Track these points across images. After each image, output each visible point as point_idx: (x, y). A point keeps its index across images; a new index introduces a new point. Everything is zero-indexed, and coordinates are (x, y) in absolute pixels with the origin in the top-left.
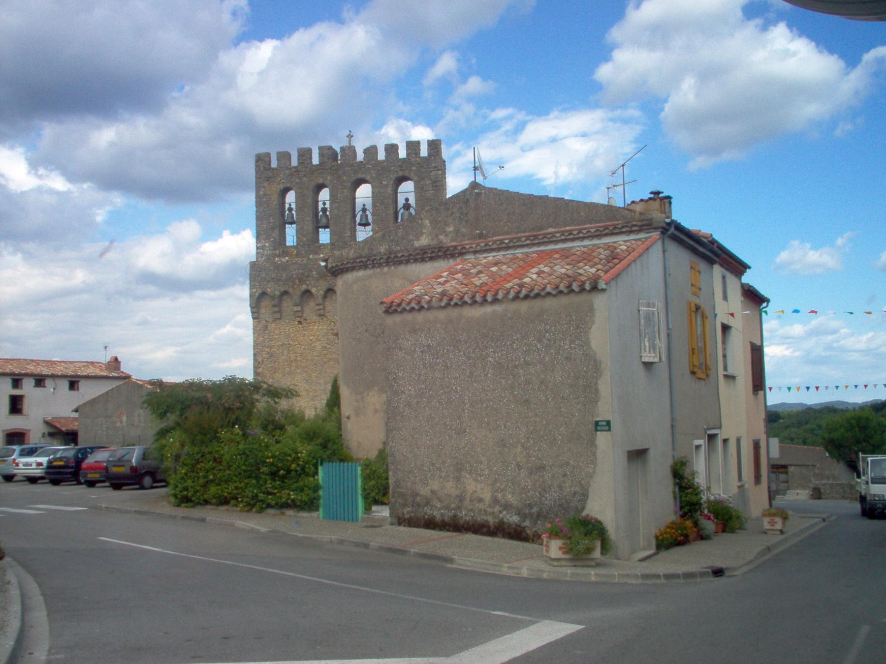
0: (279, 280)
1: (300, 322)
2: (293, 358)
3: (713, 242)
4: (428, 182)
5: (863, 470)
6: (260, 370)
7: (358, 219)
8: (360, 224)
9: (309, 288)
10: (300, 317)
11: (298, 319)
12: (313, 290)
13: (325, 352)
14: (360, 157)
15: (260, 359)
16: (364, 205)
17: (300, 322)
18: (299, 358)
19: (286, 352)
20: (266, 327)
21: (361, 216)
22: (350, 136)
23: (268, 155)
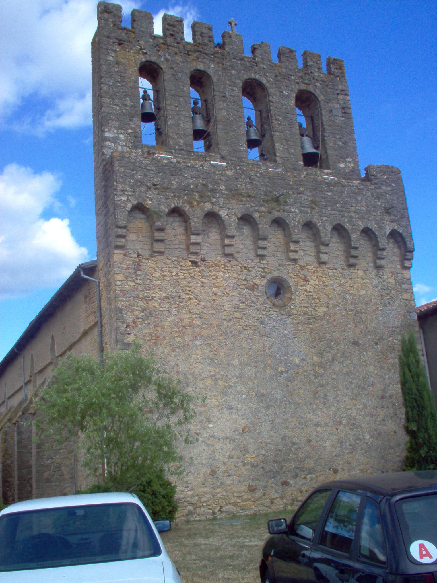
0: (166, 189)
2: (186, 322)
3: (285, 561)
4: (337, 106)
9: (216, 209)
10: (196, 254)
11: (193, 258)
12: (223, 213)
13: (237, 315)
17: (194, 263)
18: (197, 322)
19: (174, 311)
20: (138, 266)
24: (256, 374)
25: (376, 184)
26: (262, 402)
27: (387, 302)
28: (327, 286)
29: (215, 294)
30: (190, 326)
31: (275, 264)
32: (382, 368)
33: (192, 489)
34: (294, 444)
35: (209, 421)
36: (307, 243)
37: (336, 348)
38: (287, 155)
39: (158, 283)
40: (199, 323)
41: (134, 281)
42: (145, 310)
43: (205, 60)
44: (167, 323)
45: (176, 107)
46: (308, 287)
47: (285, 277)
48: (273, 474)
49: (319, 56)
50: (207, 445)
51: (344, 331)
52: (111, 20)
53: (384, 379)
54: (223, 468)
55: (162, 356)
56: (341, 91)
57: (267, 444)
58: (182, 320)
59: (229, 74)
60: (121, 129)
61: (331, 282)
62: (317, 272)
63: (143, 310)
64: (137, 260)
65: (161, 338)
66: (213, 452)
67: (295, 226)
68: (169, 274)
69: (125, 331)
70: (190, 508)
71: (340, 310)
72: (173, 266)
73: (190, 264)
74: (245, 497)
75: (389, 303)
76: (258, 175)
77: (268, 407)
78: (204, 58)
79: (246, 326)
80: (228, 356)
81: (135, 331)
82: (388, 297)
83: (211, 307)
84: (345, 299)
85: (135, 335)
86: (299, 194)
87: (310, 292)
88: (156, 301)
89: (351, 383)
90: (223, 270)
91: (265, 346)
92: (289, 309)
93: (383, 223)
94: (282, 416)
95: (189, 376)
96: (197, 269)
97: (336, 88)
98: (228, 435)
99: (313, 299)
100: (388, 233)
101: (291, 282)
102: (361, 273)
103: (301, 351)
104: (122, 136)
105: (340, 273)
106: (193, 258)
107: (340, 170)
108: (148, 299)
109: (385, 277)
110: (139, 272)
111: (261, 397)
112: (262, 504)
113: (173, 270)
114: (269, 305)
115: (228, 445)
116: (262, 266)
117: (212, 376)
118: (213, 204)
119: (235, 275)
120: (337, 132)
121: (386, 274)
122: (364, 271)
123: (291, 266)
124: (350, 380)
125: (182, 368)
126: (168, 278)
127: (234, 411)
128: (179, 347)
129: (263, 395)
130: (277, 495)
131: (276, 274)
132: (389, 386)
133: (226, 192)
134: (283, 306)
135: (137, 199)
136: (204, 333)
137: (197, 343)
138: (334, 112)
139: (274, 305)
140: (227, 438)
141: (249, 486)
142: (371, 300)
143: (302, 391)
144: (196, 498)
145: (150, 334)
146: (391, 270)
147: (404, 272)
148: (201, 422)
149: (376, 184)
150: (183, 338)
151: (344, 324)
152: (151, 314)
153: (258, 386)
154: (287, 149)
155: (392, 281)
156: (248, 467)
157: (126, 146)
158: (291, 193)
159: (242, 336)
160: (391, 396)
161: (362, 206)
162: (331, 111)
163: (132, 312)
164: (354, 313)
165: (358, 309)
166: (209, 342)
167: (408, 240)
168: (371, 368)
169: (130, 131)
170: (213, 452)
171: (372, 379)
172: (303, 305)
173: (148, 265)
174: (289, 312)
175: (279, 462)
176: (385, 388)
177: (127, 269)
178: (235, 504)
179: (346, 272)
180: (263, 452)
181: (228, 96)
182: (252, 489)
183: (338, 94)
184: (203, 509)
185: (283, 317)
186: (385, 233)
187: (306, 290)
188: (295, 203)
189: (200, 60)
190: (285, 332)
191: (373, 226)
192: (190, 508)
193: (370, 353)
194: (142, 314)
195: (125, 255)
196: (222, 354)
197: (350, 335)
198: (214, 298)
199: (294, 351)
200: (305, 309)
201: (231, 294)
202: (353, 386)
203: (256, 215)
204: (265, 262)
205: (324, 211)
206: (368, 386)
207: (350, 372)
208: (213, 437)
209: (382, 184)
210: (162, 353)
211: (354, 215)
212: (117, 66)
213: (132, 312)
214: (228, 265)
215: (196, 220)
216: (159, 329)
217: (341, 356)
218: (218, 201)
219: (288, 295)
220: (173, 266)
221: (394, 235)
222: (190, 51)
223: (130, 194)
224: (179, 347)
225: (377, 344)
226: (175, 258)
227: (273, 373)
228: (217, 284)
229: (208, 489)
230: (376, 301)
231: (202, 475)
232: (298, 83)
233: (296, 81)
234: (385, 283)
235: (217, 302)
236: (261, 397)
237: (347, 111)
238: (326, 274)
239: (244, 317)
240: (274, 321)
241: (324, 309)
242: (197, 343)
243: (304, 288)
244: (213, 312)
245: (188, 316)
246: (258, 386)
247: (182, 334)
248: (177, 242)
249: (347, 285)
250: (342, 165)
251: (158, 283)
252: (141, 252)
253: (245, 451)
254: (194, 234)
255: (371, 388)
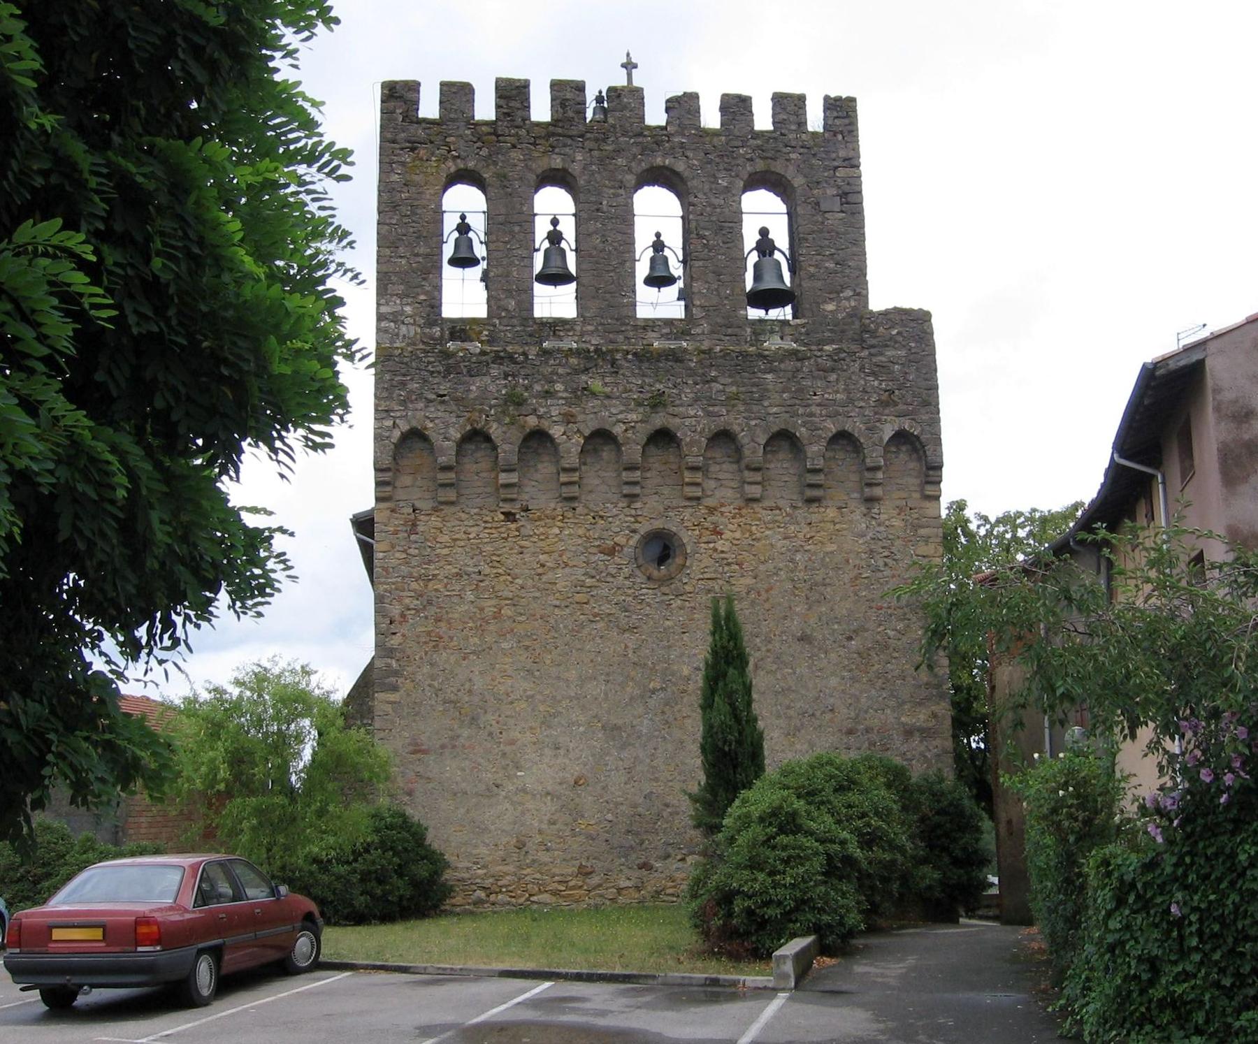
1: (509, 516)
2: (489, 611)
5: (579, 1009)
6: (395, 641)
7: (448, 251)
8: (454, 262)
9: (545, 424)
13: (578, 597)
14: (655, 116)
15: (395, 610)
16: (658, 235)
17: (509, 516)
19: (470, 596)
20: (413, 527)
21: (653, 260)
22: (629, 66)
23: (414, 87)
24: (606, 694)
25: (873, 346)
26: (614, 739)
27: (881, 563)
28: (758, 540)
29: (543, 566)
30: (495, 618)
31: (655, 511)
32: (854, 680)
33: (484, 867)
34: (667, 805)
35: (518, 768)
36: (724, 466)
37: (764, 649)
38: (715, 300)
39: (446, 551)
40: (509, 613)
41: (405, 551)
42: (421, 596)
43: (567, 150)
44: (456, 616)
45: (506, 243)
46: (720, 545)
47: (674, 529)
48: (626, 851)
49: (801, 99)
50: (513, 803)
51: (785, 618)
52: (398, 111)
53: (858, 700)
54: (539, 839)
55: (446, 666)
56: (845, 160)
57: (617, 804)
58: (482, 609)
59: (611, 167)
60: (408, 296)
61: (768, 532)
62: (741, 516)
63: (419, 596)
64: (412, 517)
65: (446, 639)
66: (523, 813)
67: (692, 443)
68: (464, 536)
69: (388, 629)
70: (482, 894)
71: (781, 581)
72: (471, 523)
73: (502, 517)
74: (571, 884)
75: (886, 565)
76: (630, 357)
77: (623, 747)
78: (565, 145)
79: (596, 615)
80: (559, 665)
81: (404, 629)
82: (886, 554)
83: (534, 587)
84: (792, 560)
85: (404, 635)
86: (708, 382)
87: (722, 552)
88: (441, 580)
89: (788, 707)
90: (559, 524)
91: (626, 647)
92: (679, 584)
93: (879, 420)
94: (648, 761)
95: (487, 697)
96: (513, 526)
97: (834, 155)
98: (549, 788)
99: (729, 564)
100: (886, 438)
101: (686, 537)
102: (831, 513)
103: (695, 655)
104: (408, 309)
105: (788, 515)
106: (507, 507)
107: (826, 317)
108: (427, 579)
109: (883, 517)
110: (413, 537)
111: (613, 730)
112: (601, 896)
113: (470, 530)
114: (640, 578)
115: (549, 804)
116: (633, 512)
117: (528, 697)
118: (540, 417)
119: (581, 532)
120: (827, 242)
121: (886, 511)
122: (840, 508)
123: (690, 510)
124: (787, 702)
125: (479, 683)
126: (462, 543)
127: (562, 752)
128: (474, 653)
129: (616, 728)
130: (628, 883)
131: (658, 524)
132: (866, 712)
133: (565, 395)
134: (670, 579)
135: (409, 422)
136: (520, 629)
137: (505, 645)
138: (824, 207)
139: (649, 578)
140: (548, 794)
141: (581, 866)
142: (848, 561)
143: (690, 721)
144: (491, 880)
145: (429, 633)
146: (898, 503)
147: (927, 504)
148: (504, 768)
149: (873, 346)
150: (482, 637)
151: (786, 605)
152: (430, 603)
153: (608, 712)
154: (716, 290)
155: (897, 523)
156: (581, 839)
157: (414, 324)
158: (690, 382)
159: (586, 631)
160: (868, 730)
161: (837, 392)
162: (818, 204)
163: (400, 600)
164: (807, 586)
165: (819, 579)
166: (527, 643)
167: (929, 449)
168: (834, 681)
169: (422, 297)
170: (523, 813)
171: (832, 700)
172: (706, 576)
173: (428, 524)
174: (677, 589)
175: (637, 834)
176: (857, 715)
177: (396, 532)
178: (555, 893)
179: (800, 514)
180: (609, 817)
181: (605, 208)
182: (585, 873)
183: (836, 168)
184: (500, 897)
185: (666, 598)
186: (881, 439)
187: (715, 550)
188: (696, 400)
189: (557, 150)
190: (668, 623)
191: (856, 426)
192: (482, 894)
193: (833, 656)
194: (416, 602)
195: (393, 511)
196: (548, 662)
197: (795, 625)
198: (540, 571)
199: (682, 655)
200: (710, 582)
201: (571, 563)
202: (791, 712)
203: (618, 430)
204: (638, 505)
205: (755, 408)
206: (824, 712)
207: (789, 689)
208: (524, 790)
209: (887, 346)
210: (447, 661)
211: (814, 409)
212: (405, 189)
213: (400, 600)
214: (570, 514)
215: (506, 447)
216: (442, 624)
217: (774, 662)
218: (549, 412)
219: (679, 560)
220: (471, 523)
221: (901, 437)
222: (539, 137)
223: (398, 414)
224: (474, 653)
225: (850, 638)
226: (476, 510)
227: (637, 692)
228: (547, 549)
229: (511, 868)
230: (857, 562)
231: (501, 847)
232: (751, 160)
233: (748, 156)
234: (882, 529)
235: (544, 578)
236: (613, 730)
237: (851, 198)
238: (760, 520)
239: (592, 601)
240: (649, 605)
241: (749, 581)
242: (505, 645)
243: (711, 545)
244: (538, 594)
245: (493, 602)
246: (608, 712)
247: (481, 630)
248: (479, 484)
249: (801, 535)
250: (830, 307)
251: (446, 551)
252: (418, 504)
253: (578, 814)
254: (504, 471)
255: (828, 716)
